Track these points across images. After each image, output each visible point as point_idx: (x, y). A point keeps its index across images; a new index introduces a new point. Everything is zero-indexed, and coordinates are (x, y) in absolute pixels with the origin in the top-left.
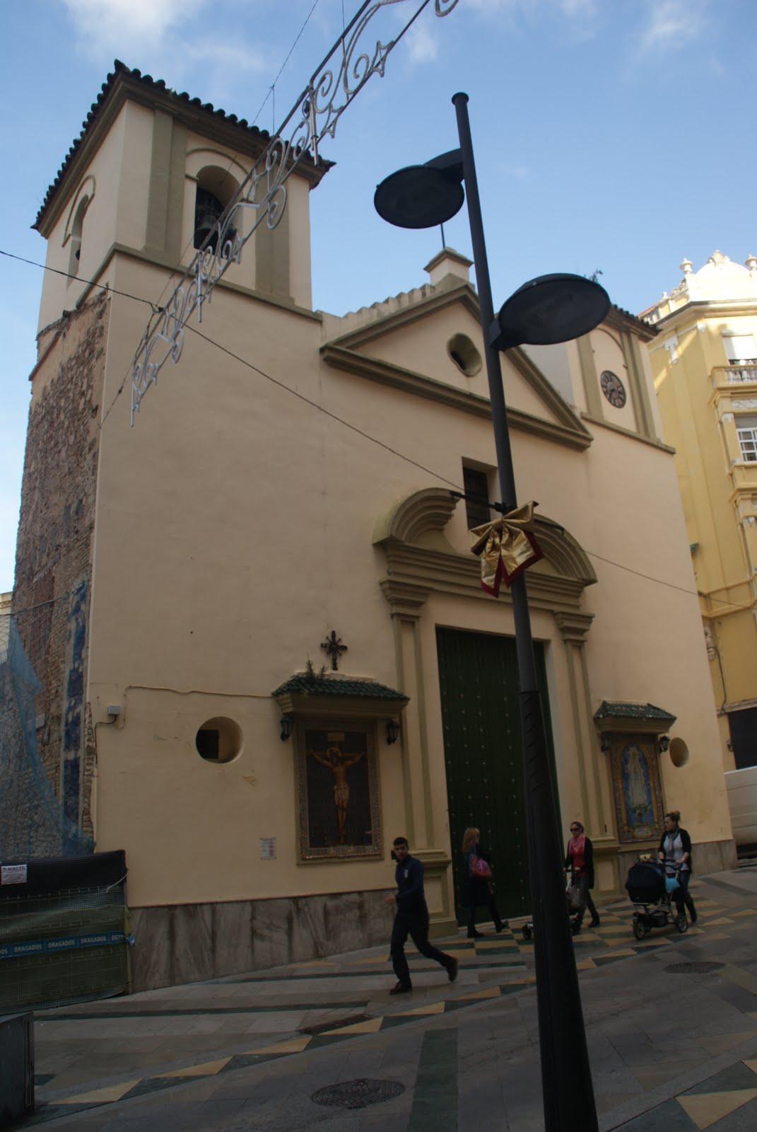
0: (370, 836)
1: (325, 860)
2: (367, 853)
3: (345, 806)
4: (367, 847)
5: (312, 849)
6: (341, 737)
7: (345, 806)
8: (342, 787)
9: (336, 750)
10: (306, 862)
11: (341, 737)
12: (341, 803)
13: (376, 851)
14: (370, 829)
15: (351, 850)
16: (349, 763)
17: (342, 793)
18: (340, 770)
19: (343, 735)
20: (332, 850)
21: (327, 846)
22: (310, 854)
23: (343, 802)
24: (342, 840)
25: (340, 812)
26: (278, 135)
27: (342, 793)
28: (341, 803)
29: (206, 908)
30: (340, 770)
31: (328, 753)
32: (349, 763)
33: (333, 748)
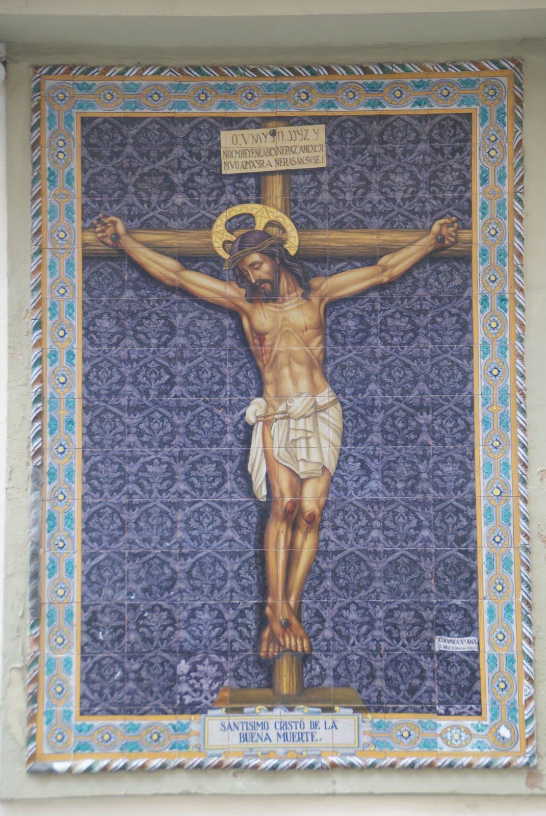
0: (469, 665)
1: (181, 782)
2: (444, 754)
3: (310, 504)
4: (444, 723)
5: (98, 722)
6: (309, 148)
7: (310, 504)
8: (298, 405)
9: (263, 215)
10: (55, 788)
11: (309, 148)
12: (283, 482)
13: (503, 745)
14: (469, 626)
15: (341, 731)
16: (351, 281)
17: (298, 435)
18: (289, 321)
19: (317, 135)
20: (216, 732)
21: (196, 709)
22: (82, 748)
23: (299, 483)
24: (285, 681)
25: (277, 532)
26: (332, 403)
27: (298, 435)
28: (283, 482)
29: (278, 179)
30: (289, 321)
31: (219, 236)
32: (351, 281)
33: (252, 208)
